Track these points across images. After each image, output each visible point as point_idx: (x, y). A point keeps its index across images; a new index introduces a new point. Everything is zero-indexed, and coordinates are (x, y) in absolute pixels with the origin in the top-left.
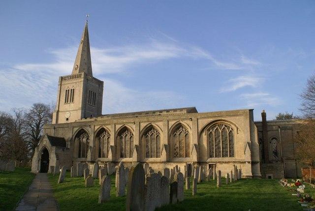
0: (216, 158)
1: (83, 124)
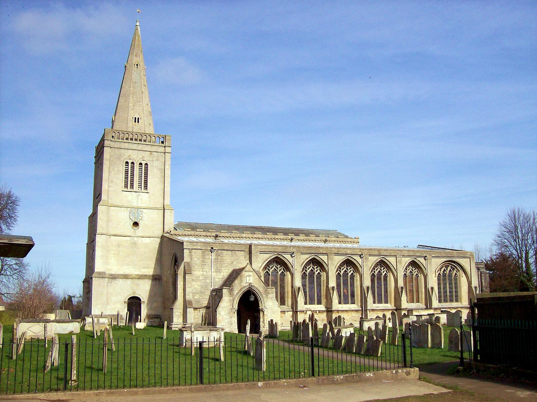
0: (445, 304)
1: (280, 250)
